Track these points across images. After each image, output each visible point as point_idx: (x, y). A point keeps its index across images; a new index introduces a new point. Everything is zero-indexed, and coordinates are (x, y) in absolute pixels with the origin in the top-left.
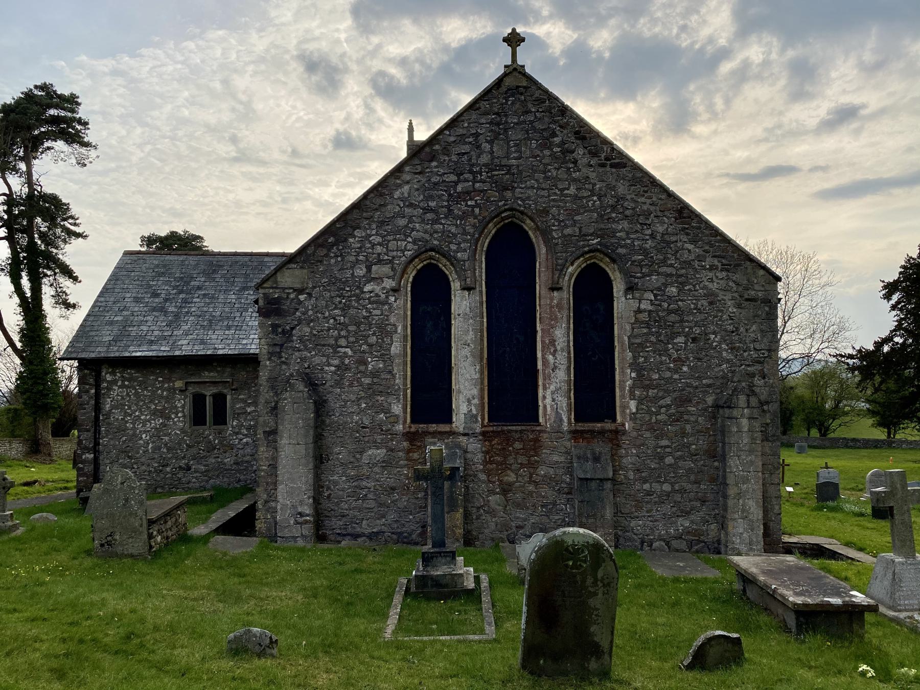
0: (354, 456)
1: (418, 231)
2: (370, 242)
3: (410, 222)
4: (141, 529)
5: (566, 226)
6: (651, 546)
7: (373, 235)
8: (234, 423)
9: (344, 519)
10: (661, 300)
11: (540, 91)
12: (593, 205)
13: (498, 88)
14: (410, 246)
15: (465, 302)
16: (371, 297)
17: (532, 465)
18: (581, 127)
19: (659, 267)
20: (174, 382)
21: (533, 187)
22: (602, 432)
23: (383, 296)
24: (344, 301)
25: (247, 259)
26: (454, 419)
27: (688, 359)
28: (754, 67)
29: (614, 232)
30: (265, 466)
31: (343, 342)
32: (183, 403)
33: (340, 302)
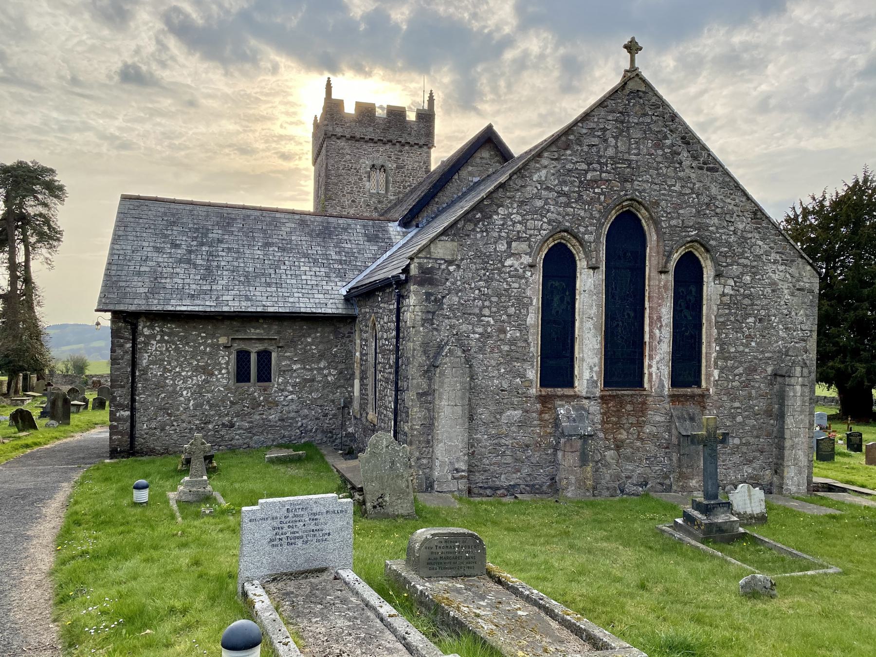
0: (495, 417)
1: (553, 212)
2: (511, 220)
3: (546, 204)
4: (407, 490)
5: (672, 218)
6: (724, 489)
7: (514, 214)
8: (280, 380)
9: (486, 474)
10: (738, 286)
11: (655, 98)
12: (693, 202)
13: (623, 90)
14: (545, 226)
15: (590, 280)
16: (511, 271)
17: (640, 425)
18: (686, 133)
19: (739, 258)
20: (217, 338)
21: (648, 181)
22: (693, 396)
23: (521, 271)
24: (488, 273)
25: (258, 213)
26: (576, 384)
27: (755, 335)
28: (532, 57)
29: (708, 226)
30: (418, 425)
31: (486, 312)
32: (227, 361)
33: (485, 275)
